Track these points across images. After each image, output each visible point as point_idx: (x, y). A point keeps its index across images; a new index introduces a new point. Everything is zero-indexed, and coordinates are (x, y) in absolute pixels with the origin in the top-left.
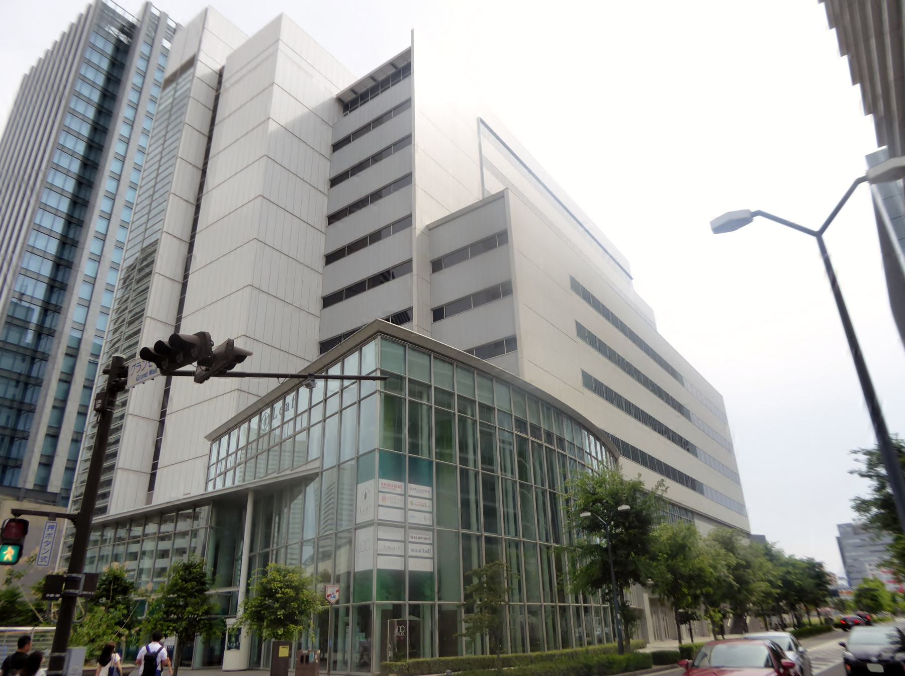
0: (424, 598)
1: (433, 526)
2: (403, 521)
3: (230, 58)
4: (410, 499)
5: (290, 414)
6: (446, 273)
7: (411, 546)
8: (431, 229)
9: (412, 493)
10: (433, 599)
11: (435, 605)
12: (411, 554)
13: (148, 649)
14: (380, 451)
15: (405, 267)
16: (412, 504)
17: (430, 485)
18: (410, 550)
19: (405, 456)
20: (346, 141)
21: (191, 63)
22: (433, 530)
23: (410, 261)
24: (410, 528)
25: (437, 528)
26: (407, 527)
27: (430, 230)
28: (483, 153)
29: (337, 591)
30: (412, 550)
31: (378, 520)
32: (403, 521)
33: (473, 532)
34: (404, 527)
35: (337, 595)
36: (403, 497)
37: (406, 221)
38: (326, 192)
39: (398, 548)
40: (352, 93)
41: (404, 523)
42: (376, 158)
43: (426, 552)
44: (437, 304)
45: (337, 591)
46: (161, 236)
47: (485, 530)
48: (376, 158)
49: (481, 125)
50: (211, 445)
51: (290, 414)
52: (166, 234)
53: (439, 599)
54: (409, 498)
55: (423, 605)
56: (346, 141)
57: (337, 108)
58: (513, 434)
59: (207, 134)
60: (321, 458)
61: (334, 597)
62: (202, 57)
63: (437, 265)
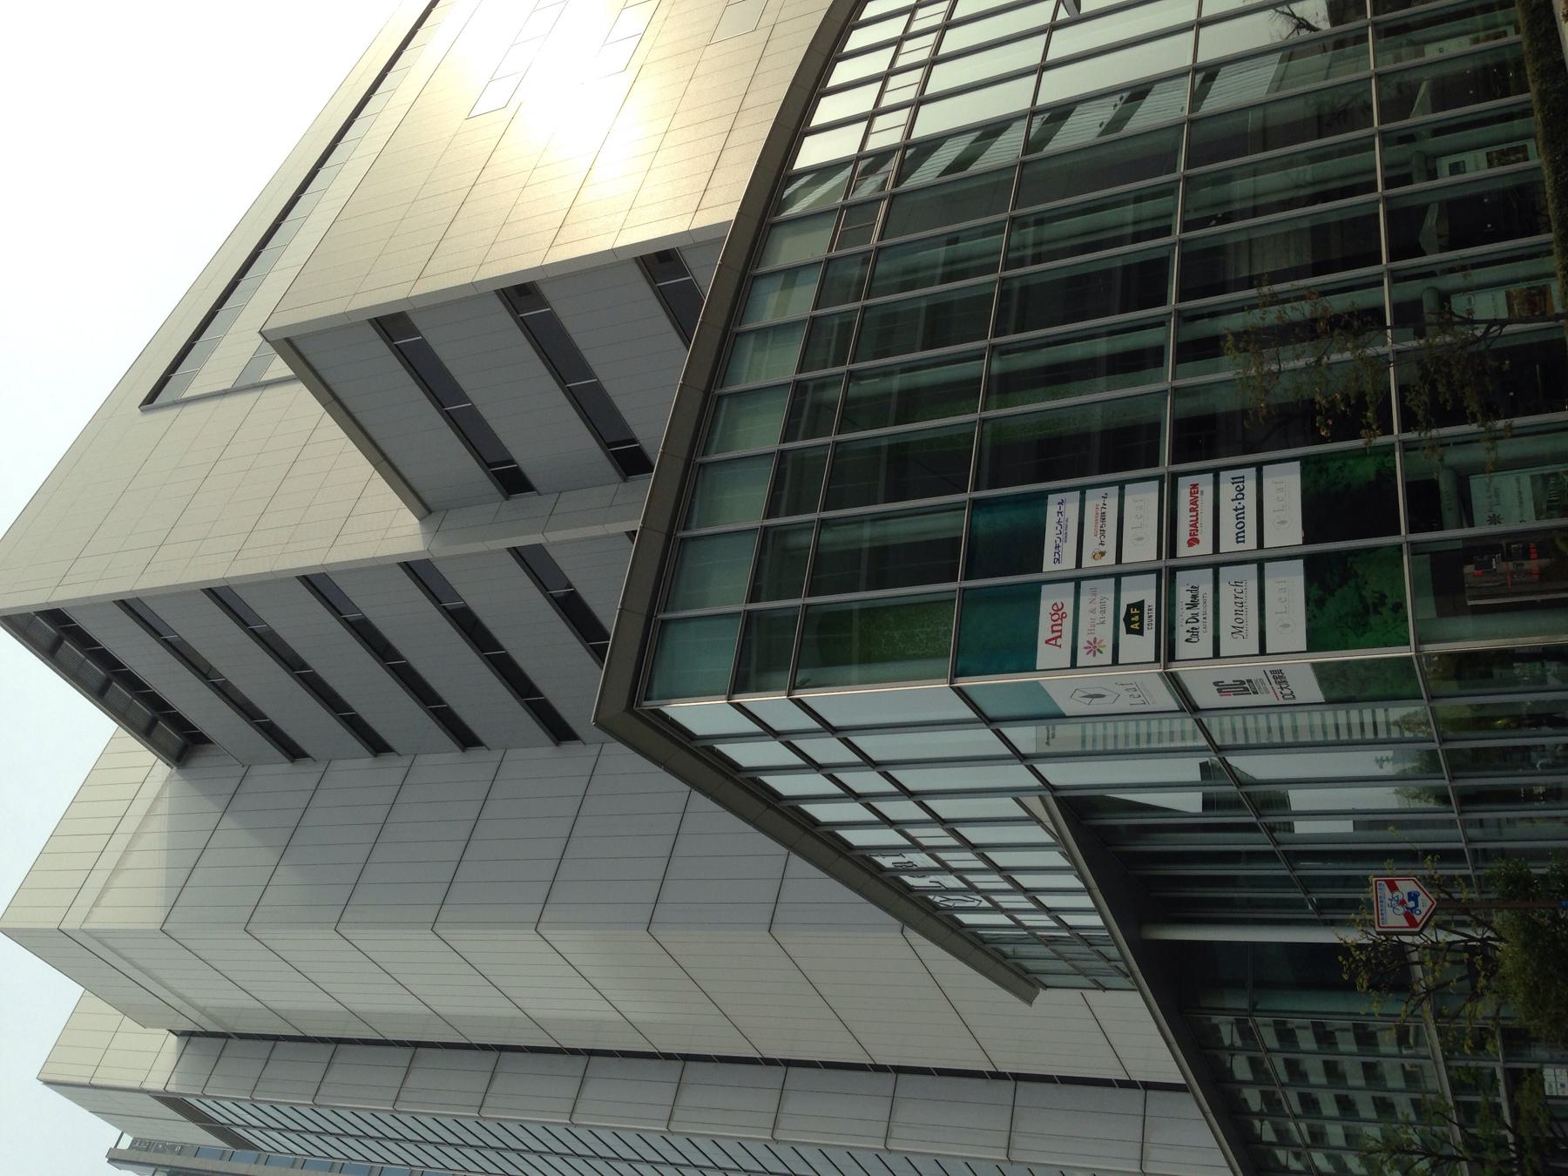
0: (1387, 476)
1: (1160, 478)
2: (1154, 576)
3: (144, 1019)
4: (1087, 562)
5: (921, 860)
6: (525, 456)
7: (1228, 544)
8: (425, 508)
9: (1069, 562)
10: (1389, 450)
11: (1412, 544)
12: (1251, 543)
13: (1431, 324)
14: (958, 673)
15: (532, 561)
16: (1103, 554)
17: (1042, 498)
18: (1241, 547)
19: (965, 590)
20: (272, 733)
21: (175, 1103)
22: (1175, 477)
23: (516, 552)
24: (1173, 553)
25: (1165, 467)
26: (1173, 562)
27: (430, 511)
28: (228, 386)
29: (1393, 887)
30: (1240, 538)
31: (1157, 659)
32: (1154, 576)
33: (1168, 337)
34: (1173, 571)
35: (1406, 887)
36: (1083, 584)
37: (417, 571)
38: (406, 761)
39: (1238, 586)
40: (155, 732)
41: (1158, 572)
42: (292, 663)
43: (1240, 491)
44: (608, 468)
45: (1393, 887)
46: (582, 1126)
47: (1162, 301)
48: (292, 663)
49: (163, 398)
50: (1046, 987)
51: (921, 860)
52: (575, 1116)
53: (1371, 187)
54: (1084, 565)
55: (1405, 475)
56: (272, 733)
57: (201, 763)
58: (879, 250)
59: (332, 1047)
60: (1015, 794)
61: (1413, 897)
62: (156, 1083)
63: (512, 481)
